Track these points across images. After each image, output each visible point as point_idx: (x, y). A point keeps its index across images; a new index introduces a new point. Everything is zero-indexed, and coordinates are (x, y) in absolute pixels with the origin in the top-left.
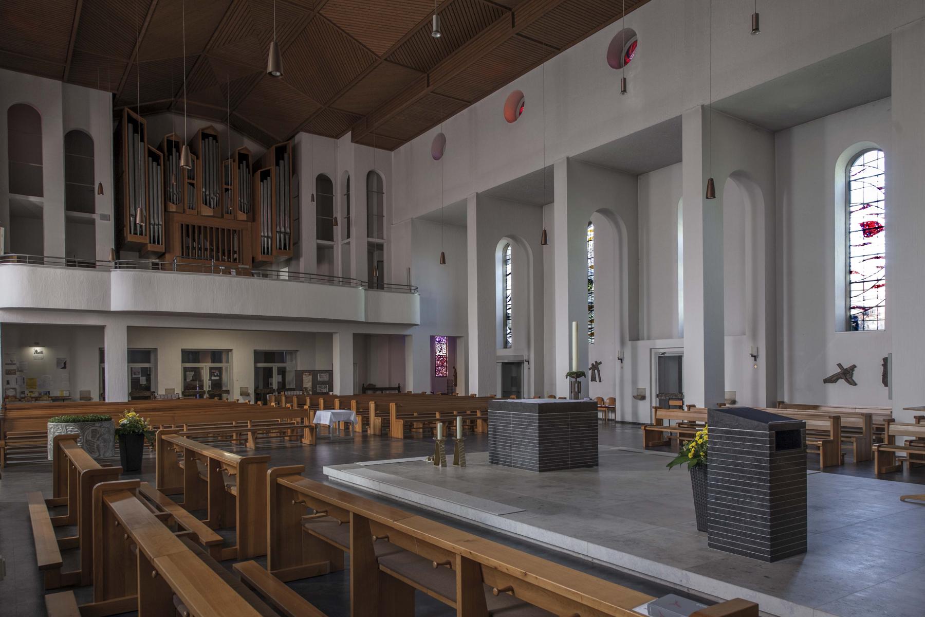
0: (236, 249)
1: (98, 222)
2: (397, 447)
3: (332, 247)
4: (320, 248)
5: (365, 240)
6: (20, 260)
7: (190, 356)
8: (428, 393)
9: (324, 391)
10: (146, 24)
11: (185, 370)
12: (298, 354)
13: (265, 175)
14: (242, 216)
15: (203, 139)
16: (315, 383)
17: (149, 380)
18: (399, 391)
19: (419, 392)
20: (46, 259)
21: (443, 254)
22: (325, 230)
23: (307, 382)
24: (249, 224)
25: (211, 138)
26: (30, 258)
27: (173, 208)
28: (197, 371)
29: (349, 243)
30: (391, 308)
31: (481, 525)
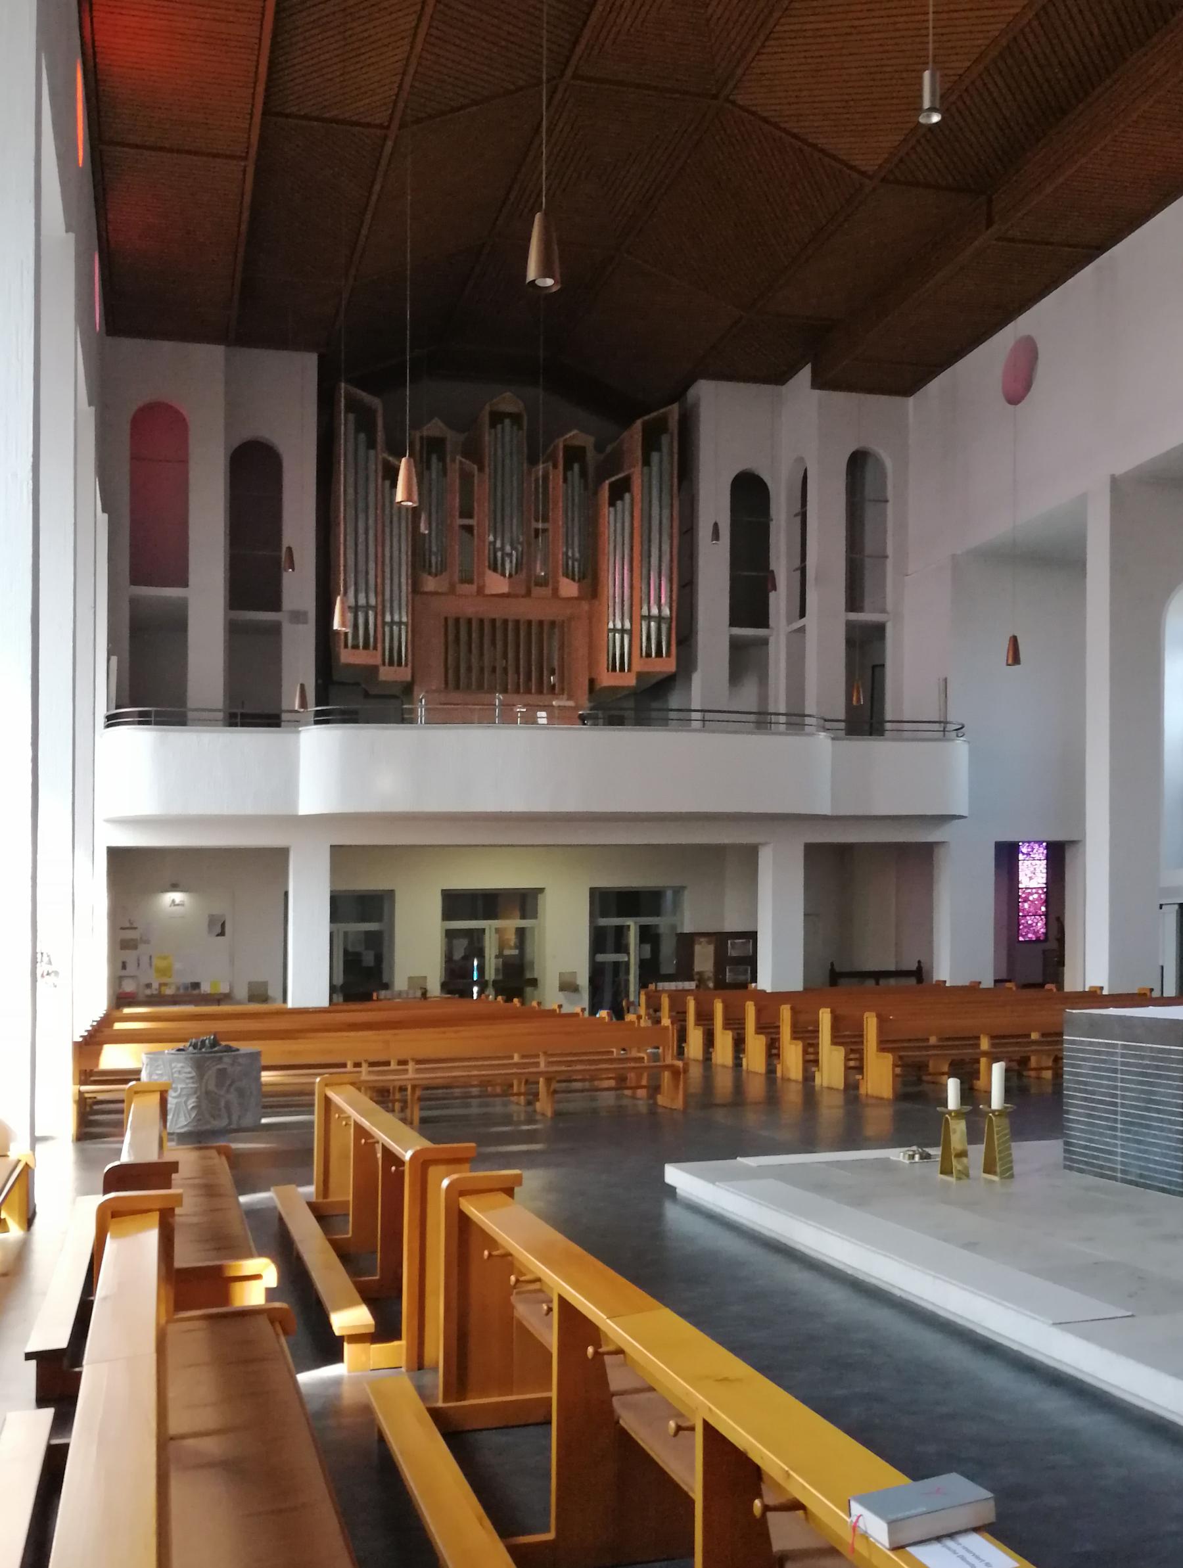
0: (556, 664)
1: (287, 629)
2: (878, 1119)
3: (765, 642)
4: (737, 648)
5: (839, 618)
6: (144, 720)
7: (457, 904)
8: (988, 982)
9: (742, 978)
10: (374, 197)
11: (450, 935)
12: (686, 893)
13: (620, 490)
14: (569, 588)
15: (493, 425)
16: (721, 961)
17: (379, 958)
18: (920, 980)
19: (963, 981)
20: (190, 715)
21: (1014, 641)
22: (750, 604)
23: (704, 959)
24: (585, 606)
25: (507, 422)
26: (157, 714)
27: (430, 584)
28: (475, 937)
29: (802, 630)
30: (890, 782)
31: (979, 1330)
